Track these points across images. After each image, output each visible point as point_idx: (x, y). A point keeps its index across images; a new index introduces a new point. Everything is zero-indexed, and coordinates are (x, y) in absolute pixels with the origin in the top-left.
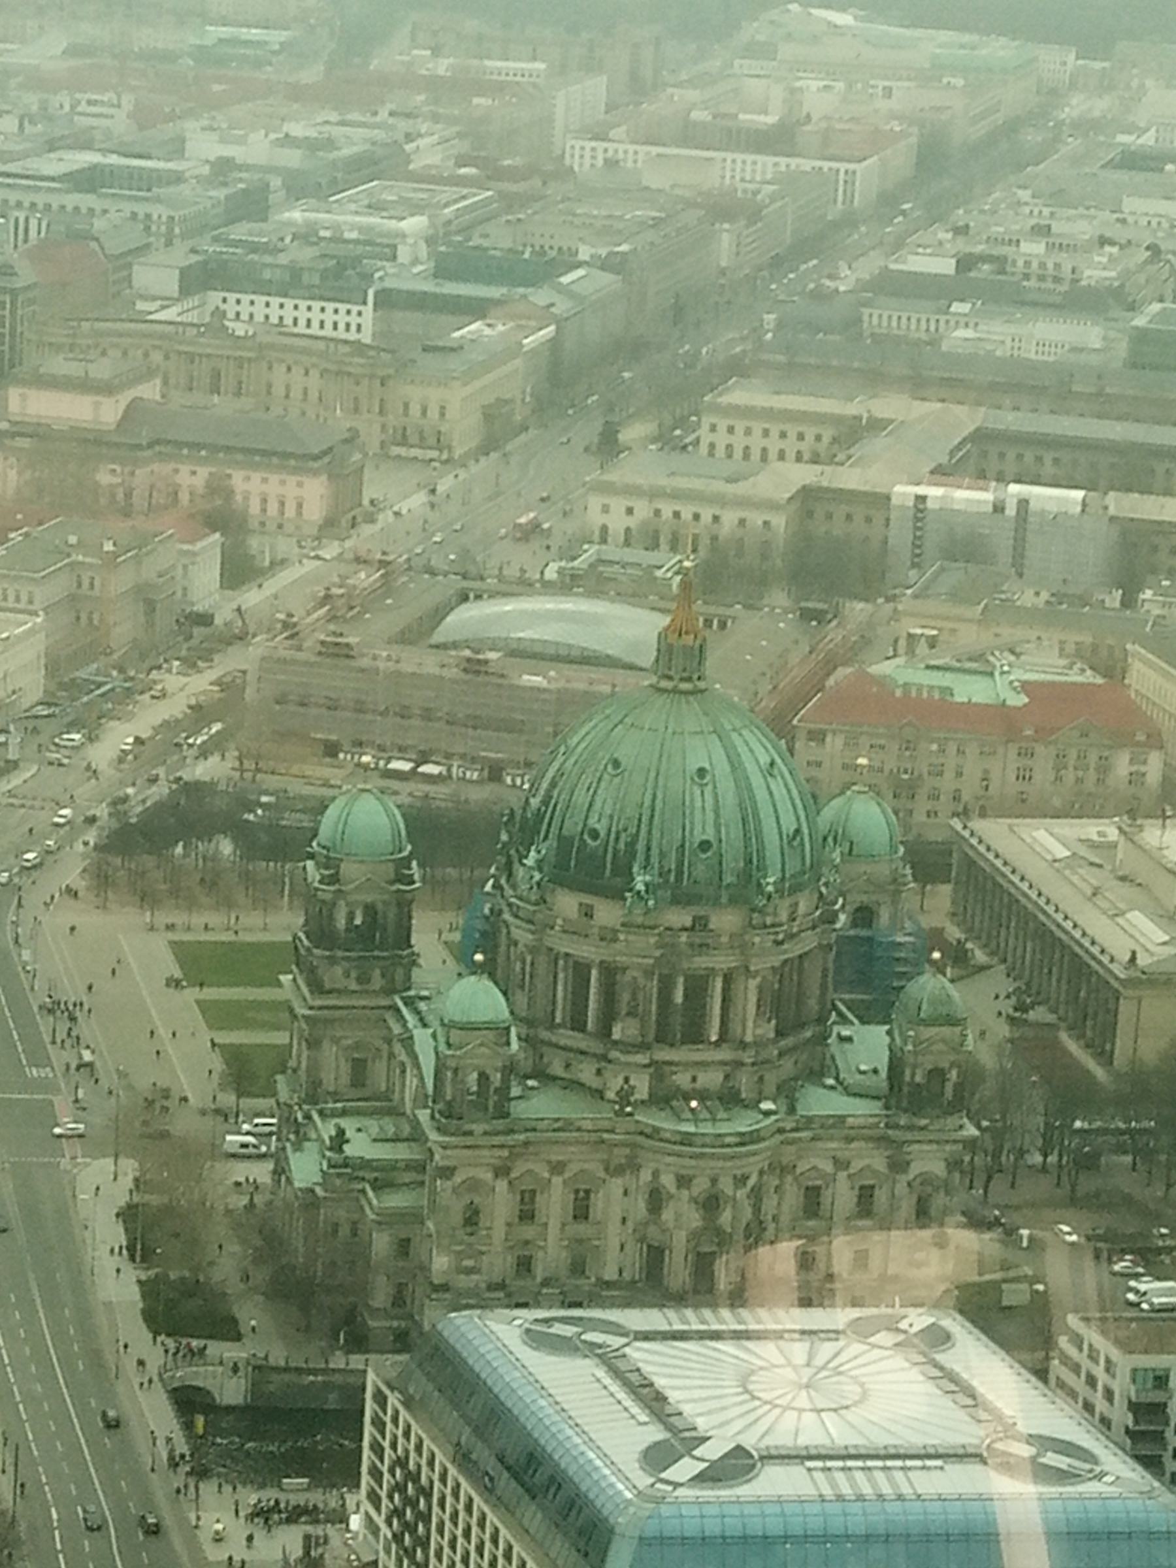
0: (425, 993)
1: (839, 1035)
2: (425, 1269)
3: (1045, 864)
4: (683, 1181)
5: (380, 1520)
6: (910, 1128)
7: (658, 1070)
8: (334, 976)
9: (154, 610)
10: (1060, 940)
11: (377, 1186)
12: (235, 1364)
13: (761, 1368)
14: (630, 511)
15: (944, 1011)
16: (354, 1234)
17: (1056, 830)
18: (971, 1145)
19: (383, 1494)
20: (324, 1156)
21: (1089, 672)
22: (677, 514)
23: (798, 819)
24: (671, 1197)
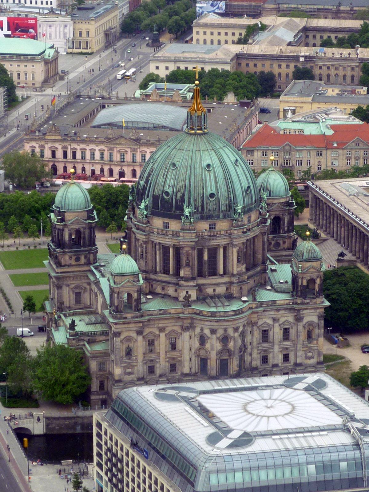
1: (271, 269)
2: (111, 374)
3: (345, 197)
4: (213, 331)
5: (103, 474)
6: (302, 304)
7: (200, 288)
8: (66, 259)
10: (355, 226)
11: (89, 342)
12: (39, 417)
13: (251, 402)
14: (167, 68)
15: (312, 256)
19: (103, 463)
20: (67, 333)
23: (248, 182)
24: (209, 338)
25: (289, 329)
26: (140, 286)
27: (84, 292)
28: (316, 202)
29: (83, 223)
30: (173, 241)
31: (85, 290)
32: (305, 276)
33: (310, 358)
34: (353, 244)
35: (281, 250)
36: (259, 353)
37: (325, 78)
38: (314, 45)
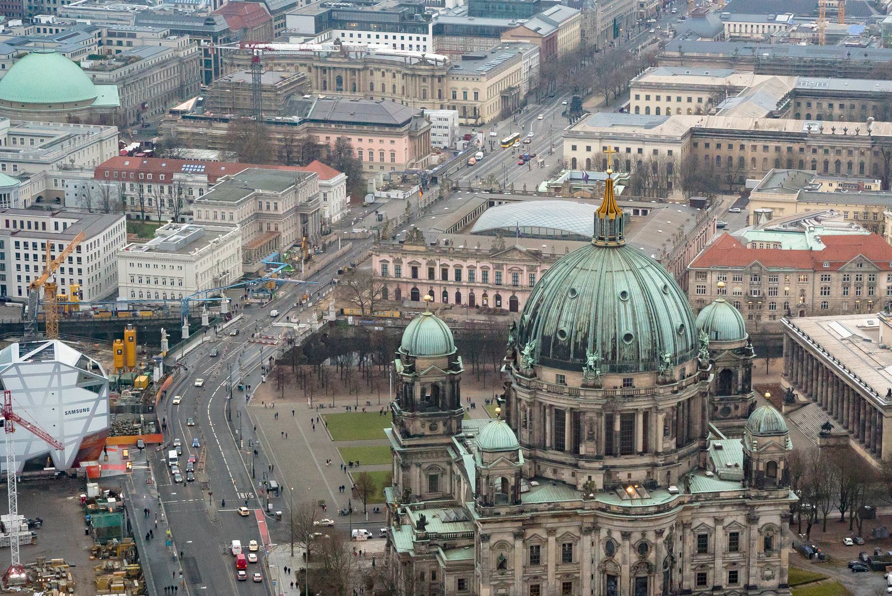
0: (470, 434)
4: (626, 535)
6: (758, 497)
7: (608, 471)
8: (416, 426)
9: (307, 221)
10: (847, 386)
11: (446, 549)
14: (589, 149)
16: (434, 578)
17: (843, 322)
18: (794, 507)
20: (414, 533)
21: (862, 229)
22: (617, 149)
25: (737, 534)
26: (521, 468)
27: (442, 474)
28: (793, 349)
29: (442, 375)
30: (571, 402)
31: (444, 473)
32: (761, 457)
33: (768, 578)
34: (845, 412)
35: (732, 418)
36: (694, 570)
37: (820, 167)
38: (808, 117)
